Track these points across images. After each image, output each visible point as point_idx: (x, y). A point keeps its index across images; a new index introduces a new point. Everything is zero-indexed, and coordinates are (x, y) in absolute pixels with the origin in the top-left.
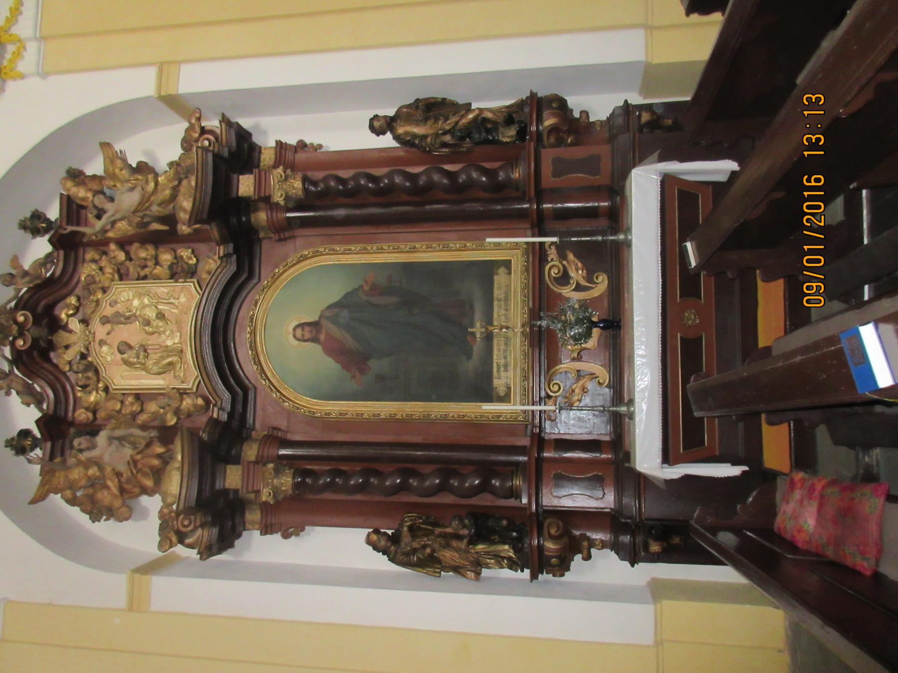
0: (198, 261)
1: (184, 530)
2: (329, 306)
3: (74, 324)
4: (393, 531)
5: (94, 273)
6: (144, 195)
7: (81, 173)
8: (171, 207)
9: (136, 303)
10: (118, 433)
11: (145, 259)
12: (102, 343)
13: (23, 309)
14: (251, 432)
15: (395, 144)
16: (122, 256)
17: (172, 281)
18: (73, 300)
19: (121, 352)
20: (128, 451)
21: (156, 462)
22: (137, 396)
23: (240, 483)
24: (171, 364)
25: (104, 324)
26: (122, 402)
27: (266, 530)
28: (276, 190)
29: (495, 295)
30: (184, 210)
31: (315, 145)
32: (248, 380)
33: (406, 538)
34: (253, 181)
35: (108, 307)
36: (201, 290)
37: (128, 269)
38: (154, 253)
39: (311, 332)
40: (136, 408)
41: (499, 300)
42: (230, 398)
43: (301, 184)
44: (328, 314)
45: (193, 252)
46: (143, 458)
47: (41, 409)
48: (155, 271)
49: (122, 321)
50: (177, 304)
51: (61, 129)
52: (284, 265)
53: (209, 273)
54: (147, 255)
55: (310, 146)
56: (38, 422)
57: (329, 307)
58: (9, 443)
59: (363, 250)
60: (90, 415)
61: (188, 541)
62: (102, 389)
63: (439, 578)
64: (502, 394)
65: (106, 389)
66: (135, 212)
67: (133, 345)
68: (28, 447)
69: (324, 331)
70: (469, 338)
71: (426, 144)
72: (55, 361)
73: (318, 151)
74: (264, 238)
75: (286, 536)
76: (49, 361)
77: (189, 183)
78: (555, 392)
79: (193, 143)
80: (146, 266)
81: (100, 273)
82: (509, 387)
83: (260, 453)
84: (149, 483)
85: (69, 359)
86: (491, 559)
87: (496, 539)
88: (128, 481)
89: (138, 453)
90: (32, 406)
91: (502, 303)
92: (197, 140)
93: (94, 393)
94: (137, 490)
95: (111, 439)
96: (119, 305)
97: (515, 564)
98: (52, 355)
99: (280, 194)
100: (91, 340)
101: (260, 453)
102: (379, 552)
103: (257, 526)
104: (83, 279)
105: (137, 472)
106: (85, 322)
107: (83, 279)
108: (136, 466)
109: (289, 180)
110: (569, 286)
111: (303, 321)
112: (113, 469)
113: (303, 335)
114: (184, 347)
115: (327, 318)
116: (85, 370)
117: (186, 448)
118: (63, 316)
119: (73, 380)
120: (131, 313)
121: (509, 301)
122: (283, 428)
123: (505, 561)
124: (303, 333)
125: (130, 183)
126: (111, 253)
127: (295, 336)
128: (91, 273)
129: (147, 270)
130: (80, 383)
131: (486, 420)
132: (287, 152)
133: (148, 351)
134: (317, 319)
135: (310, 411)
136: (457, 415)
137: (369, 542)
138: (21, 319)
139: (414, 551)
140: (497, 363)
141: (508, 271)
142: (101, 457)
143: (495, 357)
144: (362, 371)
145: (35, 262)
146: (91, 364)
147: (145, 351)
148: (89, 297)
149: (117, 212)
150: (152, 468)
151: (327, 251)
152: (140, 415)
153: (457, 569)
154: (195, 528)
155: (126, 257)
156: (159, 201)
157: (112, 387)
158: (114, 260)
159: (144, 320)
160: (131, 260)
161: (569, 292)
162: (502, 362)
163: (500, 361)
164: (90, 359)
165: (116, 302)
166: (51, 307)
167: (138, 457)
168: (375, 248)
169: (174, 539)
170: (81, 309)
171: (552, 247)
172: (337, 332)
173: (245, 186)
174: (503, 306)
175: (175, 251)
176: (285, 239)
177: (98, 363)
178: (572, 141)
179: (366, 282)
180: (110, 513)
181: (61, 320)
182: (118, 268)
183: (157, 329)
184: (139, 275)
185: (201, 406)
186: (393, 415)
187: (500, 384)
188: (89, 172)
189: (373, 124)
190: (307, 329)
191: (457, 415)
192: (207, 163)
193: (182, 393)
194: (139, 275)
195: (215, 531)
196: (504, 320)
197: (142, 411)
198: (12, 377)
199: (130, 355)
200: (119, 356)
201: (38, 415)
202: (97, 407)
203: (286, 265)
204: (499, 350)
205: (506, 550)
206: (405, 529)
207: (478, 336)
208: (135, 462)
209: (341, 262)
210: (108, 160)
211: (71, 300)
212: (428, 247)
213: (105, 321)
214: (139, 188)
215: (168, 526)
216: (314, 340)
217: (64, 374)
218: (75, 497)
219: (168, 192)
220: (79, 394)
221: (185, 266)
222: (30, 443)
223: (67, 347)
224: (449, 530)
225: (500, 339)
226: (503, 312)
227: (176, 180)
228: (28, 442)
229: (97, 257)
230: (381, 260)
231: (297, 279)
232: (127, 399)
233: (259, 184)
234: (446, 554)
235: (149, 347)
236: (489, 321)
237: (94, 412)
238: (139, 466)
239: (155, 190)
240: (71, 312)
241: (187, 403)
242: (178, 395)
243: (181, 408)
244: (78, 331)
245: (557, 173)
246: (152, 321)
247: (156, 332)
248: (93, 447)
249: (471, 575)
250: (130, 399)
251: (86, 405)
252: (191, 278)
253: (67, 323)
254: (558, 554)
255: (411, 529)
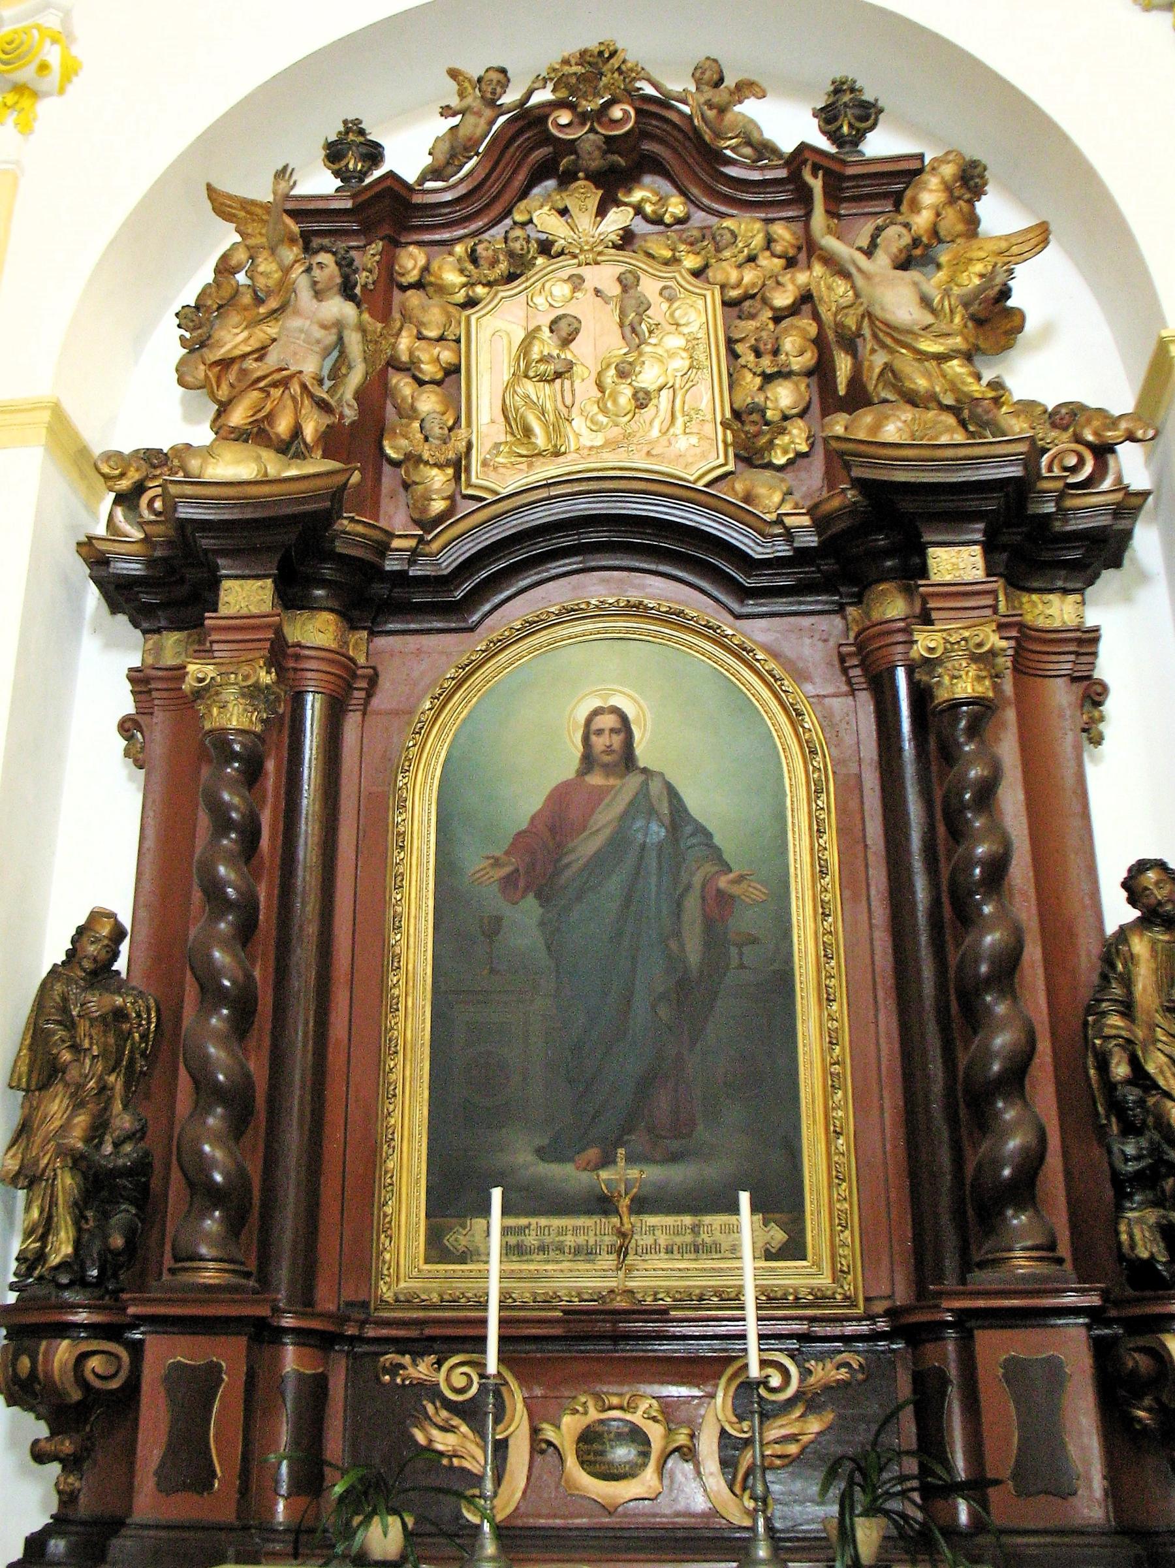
0: (780, 468)
1: (144, 501)
2: (673, 788)
3: (617, 219)
4: (124, 975)
5: (740, 245)
6: (909, 332)
7: (978, 192)
8: (885, 394)
9: (674, 342)
10: (354, 341)
11: (776, 352)
12: (577, 282)
13: (639, 112)
14: (364, 628)
15: (1111, 928)
16: (782, 300)
17: (728, 415)
18: (676, 207)
19: (553, 326)
20: (309, 366)
21: (283, 427)
22: (453, 371)
23: (231, 611)
24: (528, 432)
25: (619, 280)
26: (441, 338)
27: (139, 680)
28: (945, 635)
29: (707, 1219)
30: (877, 427)
31: (1102, 726)
32: (491, 612)
33: (98, 1002)
34: (968, 578)
35: (662, 284)
36: (707, 485)
37: (752, 317)
38: (795, 367)
39: (609, 750)
40: (429, 370)
41: (695, 1229)
42: (440, 573)
43: (965, 695)
44: (655, 787)
45: (800, 455)
46: (293, 398)
47: (423, 179)
48: (749, 376)
49: (627, 317)
50: (672, 431)
51: (1065, 139)
52: (775, 672)
53: (748, 499)
54: (787, 354)
55: (1096, 714)
56: (391, 175)
57: (672, 792)
58: (354, 128)
59: (820, 866)
60: (413, 277)
61: (119, 512)
62: (471, 293)
63: (6, 1084)
64: (449, 1240)
65: (471, 303)
66: (869, 315)
67: (572, 346)
68: (343, 163)
69: (612, 781)
70: (593, 1153)
71: (1104, 1014)
72: (536, 191)
73: (1085, 735)
74: (844, 618)
75: (127, 727)
76: (536, 178)
77: (949, 430)
78: (448, 1379)
79: (1071, 430)
80: (758, 354)
81: (741, 258)
82: (466, 1258)
83: (307, 652)
84: (238, 417)
85: (535, 220)
86: (41, 1213)
87: (87, 1221)
88: (244, 372)
89: (304, 387)
90: (430, 159)
91: (688, 1238)
92: (1078, 439)
93: (464, 279)
94: (223, 393)
95: (339, 326)
96: (665, 306)
97: (28, 1268)
98: (551, 183)
99: (932, 645)
100: (581, 257)
101: (307, 652)
102: (73, 942)
103: (150, 661)
104: (727, 223)
105: (261, 389)
106: (627, 239)
107: (724, 225)
108: (275, 385)
109: (974, 666)
110: (734, 1419)
111: (634, 728)
112: (274, 340)
113: (600, 732)
114: (569, 457)
115: (644, 788)
116: (511, 254)
117: (319, 483)
118: (637, 195)
119: (493, 231)
120: (647, 334)
121: (693, 1256)
122: (375, 702)
123: (38, 1244)
124: (607, 732)
125: (942, 299)
126: (789, 276)
127: (597, 712)
128: (739, 238)
129: (751, 357)
130: (480, 248)
131: (380, 1198)
132: (1072, 657)
133: (558, 381)
134: (641, 764)
135: (410, 760)
136: (394, 1126)
137: (96, 916)
138: (617, 113)
139: (70, 1025)
140: (528, 1226)
141: (773, 1251)
142: (297, 313)
143: (543, 1221)
144: (509, 882)
145: (752, 121)
146: (531, 264)
147: (558, 375)
148: (684, 242)
149: (867, 276)
150: (270, 418)
151: (816, 776)
152: (410, 380)
153: (24, 1131)
154: (141, 525)
155: (780, 309)
156: (898, 364)
157: (474, 314)
158: (774, 285)
159: (630, 364)
160: (777, 320)
161: (719, 1421)
162: (531, 1240)
163: (533, 1233)
164: (540, 261)
165: (671, 300)
166: (658, 167)
167: (295, 388)
168: (827, 897)
169: (124, 484)
170: (661, 228)
171: (843, 1370)
172: (606, 816)
173: (954, 560)
174: (678, 1240)
175: (802, 415)
176: (845, 671)
177: (527, 280)
178: (1139, 1420)
179: (741, 878)
180: (196, 345)
181: (629, 191)
182: (756, 294)
183: (610, 396)
184: (737, 341)
185: (425, 510)
186: (396, 964)
187: (473, 1236)
188: (983, 207)
189: (1148, 869)
190: (617, 741)
191: (394, 1126)
192: (977, 467)
193: (459, 466)
194: (737, 341)
195: (135, 568)
196: (640, 1243)
197: (421, 383)
198: (488, 113)
199: (546, 344)
200: (545, 321)
201: (411, 177)
202: (430, 289)
203: (773, 676)
204: (562, 1231)
205: (62, 1247)
206: (119, 1001)
207: (604, 1174)
208: (284, 383)
209: (789, 813)
210: (1004, 245)
211: (676, 205)
212: (833, 1034)
213: (627, 283)
214: (929, 319)
215: (155, 467)
216: (588, 761)
217: (508, 213)
218: (234, 271)
219: (921, 383)
220: (459, 249)
221: (763, 440)
222: (351, 166)
223: (564, 212)
224: (118, 1106)
225: (592, 1233)
226: (663, 1240)
227: (957, 400)
228: (353, 164)
229: (778, 248)
230: (798, 915)
231: (745, 707)
232: (448, 348)
233: (959, 592)
234: (57, 1101)
235: (567, 383)
236: (642, 1205)
237: (419, 285)
238: (276, 393)
239: (923, 356)
240: (649, 209)
241: (438, 479)
242: (451, 455)
243: (422, 466)
244: (602, 228)
245: (1015, 1371)
246: (629, 381)
247: (603, 391)
248: (319, 294)
249: (13, 1165)
250: (447, 356)
251: (435, 266)
252: (736, 456)
253: (619, 204)
254: (41, 1376)
255: (120, 1014)
